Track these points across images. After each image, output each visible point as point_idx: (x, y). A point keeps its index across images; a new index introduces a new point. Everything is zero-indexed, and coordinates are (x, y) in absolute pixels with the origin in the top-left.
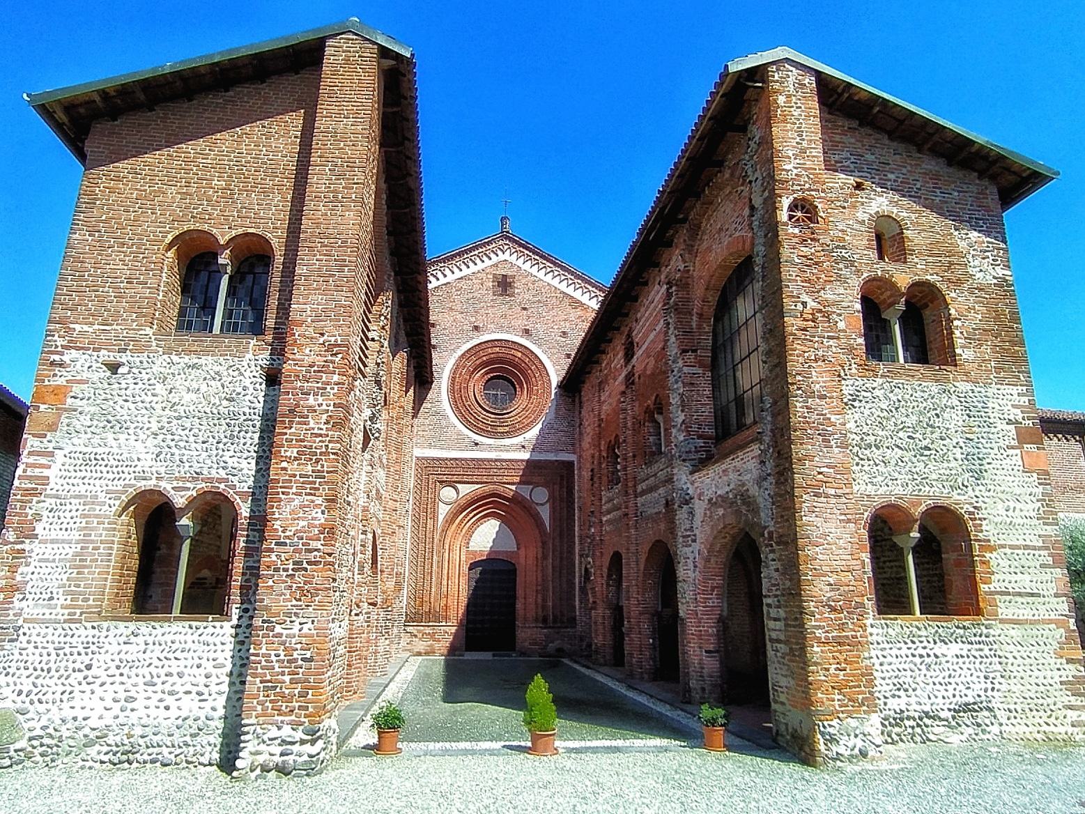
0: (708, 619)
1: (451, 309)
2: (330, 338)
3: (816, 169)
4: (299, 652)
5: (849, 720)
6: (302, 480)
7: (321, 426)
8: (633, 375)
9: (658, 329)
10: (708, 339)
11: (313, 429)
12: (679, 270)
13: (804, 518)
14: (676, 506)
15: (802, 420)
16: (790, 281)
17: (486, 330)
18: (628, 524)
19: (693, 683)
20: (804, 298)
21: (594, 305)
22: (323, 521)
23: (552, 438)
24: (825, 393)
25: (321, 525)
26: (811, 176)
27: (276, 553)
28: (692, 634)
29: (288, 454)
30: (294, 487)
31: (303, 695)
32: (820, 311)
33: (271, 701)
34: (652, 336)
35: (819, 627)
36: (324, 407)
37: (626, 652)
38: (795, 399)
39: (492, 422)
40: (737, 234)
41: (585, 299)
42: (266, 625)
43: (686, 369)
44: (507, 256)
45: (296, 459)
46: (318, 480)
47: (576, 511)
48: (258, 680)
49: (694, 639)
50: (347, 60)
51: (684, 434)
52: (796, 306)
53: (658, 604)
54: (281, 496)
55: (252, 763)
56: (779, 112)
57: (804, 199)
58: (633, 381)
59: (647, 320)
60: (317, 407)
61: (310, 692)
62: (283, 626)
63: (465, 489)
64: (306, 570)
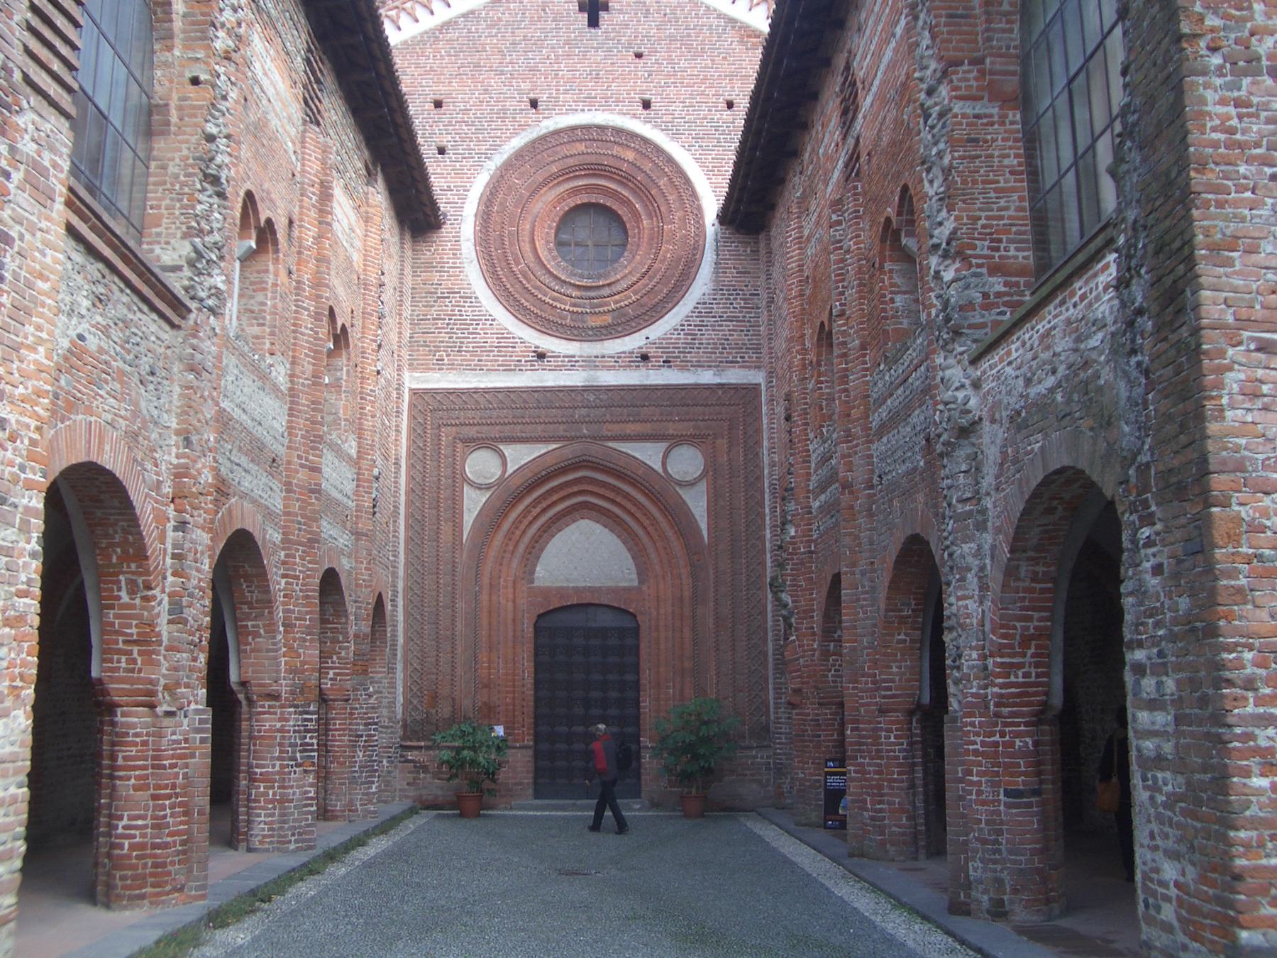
0: (1012, 715)
1: (477, 66)
10: (1011, 31)
13: (1229, 414)
15: (1222, 137)
17: (555, 105)
19: (975, 870)
23: (708, 336)
28: (976, 752)
34: (888, 54)
38: (1201, 80)
39: (574, 305)
43: (958, 108)
47: (767, 496)
51: (957, 265)
53: (920, 688)
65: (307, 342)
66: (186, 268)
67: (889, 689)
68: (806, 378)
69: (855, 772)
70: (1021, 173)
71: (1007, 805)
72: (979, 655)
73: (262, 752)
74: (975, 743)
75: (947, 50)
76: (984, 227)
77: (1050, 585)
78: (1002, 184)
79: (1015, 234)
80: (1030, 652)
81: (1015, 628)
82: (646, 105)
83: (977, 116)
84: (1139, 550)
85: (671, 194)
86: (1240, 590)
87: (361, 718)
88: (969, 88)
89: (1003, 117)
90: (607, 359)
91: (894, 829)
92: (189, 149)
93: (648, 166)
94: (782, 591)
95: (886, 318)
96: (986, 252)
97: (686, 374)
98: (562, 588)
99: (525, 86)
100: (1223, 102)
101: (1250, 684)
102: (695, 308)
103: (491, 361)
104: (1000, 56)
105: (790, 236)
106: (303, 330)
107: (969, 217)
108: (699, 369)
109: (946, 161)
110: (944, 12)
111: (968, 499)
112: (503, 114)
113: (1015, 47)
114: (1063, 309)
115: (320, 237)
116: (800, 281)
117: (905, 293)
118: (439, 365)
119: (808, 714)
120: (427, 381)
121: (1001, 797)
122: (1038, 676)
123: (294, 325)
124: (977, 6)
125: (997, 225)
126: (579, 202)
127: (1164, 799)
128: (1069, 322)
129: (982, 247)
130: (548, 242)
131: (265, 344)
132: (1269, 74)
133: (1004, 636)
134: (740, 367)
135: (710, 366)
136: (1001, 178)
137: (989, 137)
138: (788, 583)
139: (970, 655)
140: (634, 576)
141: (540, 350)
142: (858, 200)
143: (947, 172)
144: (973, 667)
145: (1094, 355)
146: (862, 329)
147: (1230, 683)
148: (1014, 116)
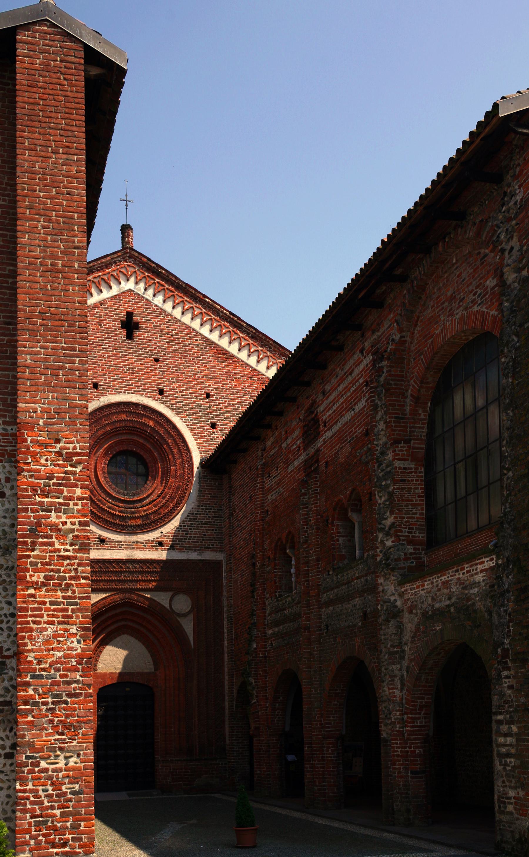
0: (415, 739)
2: (67, 445)
7: (68, 547)
8: (317, 461)
9: (358, 408)
10: (423, 428)
11: (59, 550)
12: (393, 340)
14: (380, 620)
18: (309, 639)
22: (79, 651)
25: (78, 655)
27: (32, 687)
28: (398, 756)
29: (34, 579)
30: (45, 616)
31: (75, 828)
33: (44, 835)
34: (347, 417)
36: (69, 526)
37: (306, 780)
39: (121, 512)
40: (475, 308)
42: (30, 761)
43: (397, 464)
44: (130, 285)
45: (44, 584)
46: (70, 607)
47: (225, 623)
48: (28, 815)
49: (399, 760)
50: (46, 64)
51: (393, 539)
54: (32, 625)
58: (317, 468)
59: (340, 395)
60: (61, 526)
61: (82, 823)
62: (49, 761)
64: (66, 702)
67: (329, 727)
68: (264, 565)
69: (309, 768)
71: (412, 778)
72: (400, 714)
74: (397, 751)
75: (393, 434)
76: (406, 522)
77: (432, 684)
78: (414, 502)
80: (423, 712)
81: (417, 702)
82: (161, 392)
83: (405, 469)
84: (502, 680)
85: (175, 449)
89: (416, 469)
90: (139, 544)
91: (331, 794)
93: (161, 431)
94: (249, 677)
95: (334, 549)
96: (406, 534)
97: (183, 554)
98: (112, 673)
102: (188, 516)
104: (418, 440)
107: (400, 517)
108: (190, 551)
109: (391, 489)
110: (393, 416)
111: (396, 646)
113: (424, 436)
114: (457, 574)
116: (262, 512)
117: (343, 536)
119: (263, 740)
121: (409, 774)
122: (425, 722)
124: (408, 414)
125: (412, 521)
126: (121, 449)
127: (510, 768)
128: (459, 579)
130: (104, 473)
133: (413, 706)
134: (211, 551)
135: (195, 550)
136: (414, 499)
137: (410, 479)
138: (253, 672)
139: (396, 714)
140: (152, 666)
141: (102, 537)
142: (317, 484)
143: (391, 494)
144: (397, 719)
145: (473, 597)
146: (318, 551)
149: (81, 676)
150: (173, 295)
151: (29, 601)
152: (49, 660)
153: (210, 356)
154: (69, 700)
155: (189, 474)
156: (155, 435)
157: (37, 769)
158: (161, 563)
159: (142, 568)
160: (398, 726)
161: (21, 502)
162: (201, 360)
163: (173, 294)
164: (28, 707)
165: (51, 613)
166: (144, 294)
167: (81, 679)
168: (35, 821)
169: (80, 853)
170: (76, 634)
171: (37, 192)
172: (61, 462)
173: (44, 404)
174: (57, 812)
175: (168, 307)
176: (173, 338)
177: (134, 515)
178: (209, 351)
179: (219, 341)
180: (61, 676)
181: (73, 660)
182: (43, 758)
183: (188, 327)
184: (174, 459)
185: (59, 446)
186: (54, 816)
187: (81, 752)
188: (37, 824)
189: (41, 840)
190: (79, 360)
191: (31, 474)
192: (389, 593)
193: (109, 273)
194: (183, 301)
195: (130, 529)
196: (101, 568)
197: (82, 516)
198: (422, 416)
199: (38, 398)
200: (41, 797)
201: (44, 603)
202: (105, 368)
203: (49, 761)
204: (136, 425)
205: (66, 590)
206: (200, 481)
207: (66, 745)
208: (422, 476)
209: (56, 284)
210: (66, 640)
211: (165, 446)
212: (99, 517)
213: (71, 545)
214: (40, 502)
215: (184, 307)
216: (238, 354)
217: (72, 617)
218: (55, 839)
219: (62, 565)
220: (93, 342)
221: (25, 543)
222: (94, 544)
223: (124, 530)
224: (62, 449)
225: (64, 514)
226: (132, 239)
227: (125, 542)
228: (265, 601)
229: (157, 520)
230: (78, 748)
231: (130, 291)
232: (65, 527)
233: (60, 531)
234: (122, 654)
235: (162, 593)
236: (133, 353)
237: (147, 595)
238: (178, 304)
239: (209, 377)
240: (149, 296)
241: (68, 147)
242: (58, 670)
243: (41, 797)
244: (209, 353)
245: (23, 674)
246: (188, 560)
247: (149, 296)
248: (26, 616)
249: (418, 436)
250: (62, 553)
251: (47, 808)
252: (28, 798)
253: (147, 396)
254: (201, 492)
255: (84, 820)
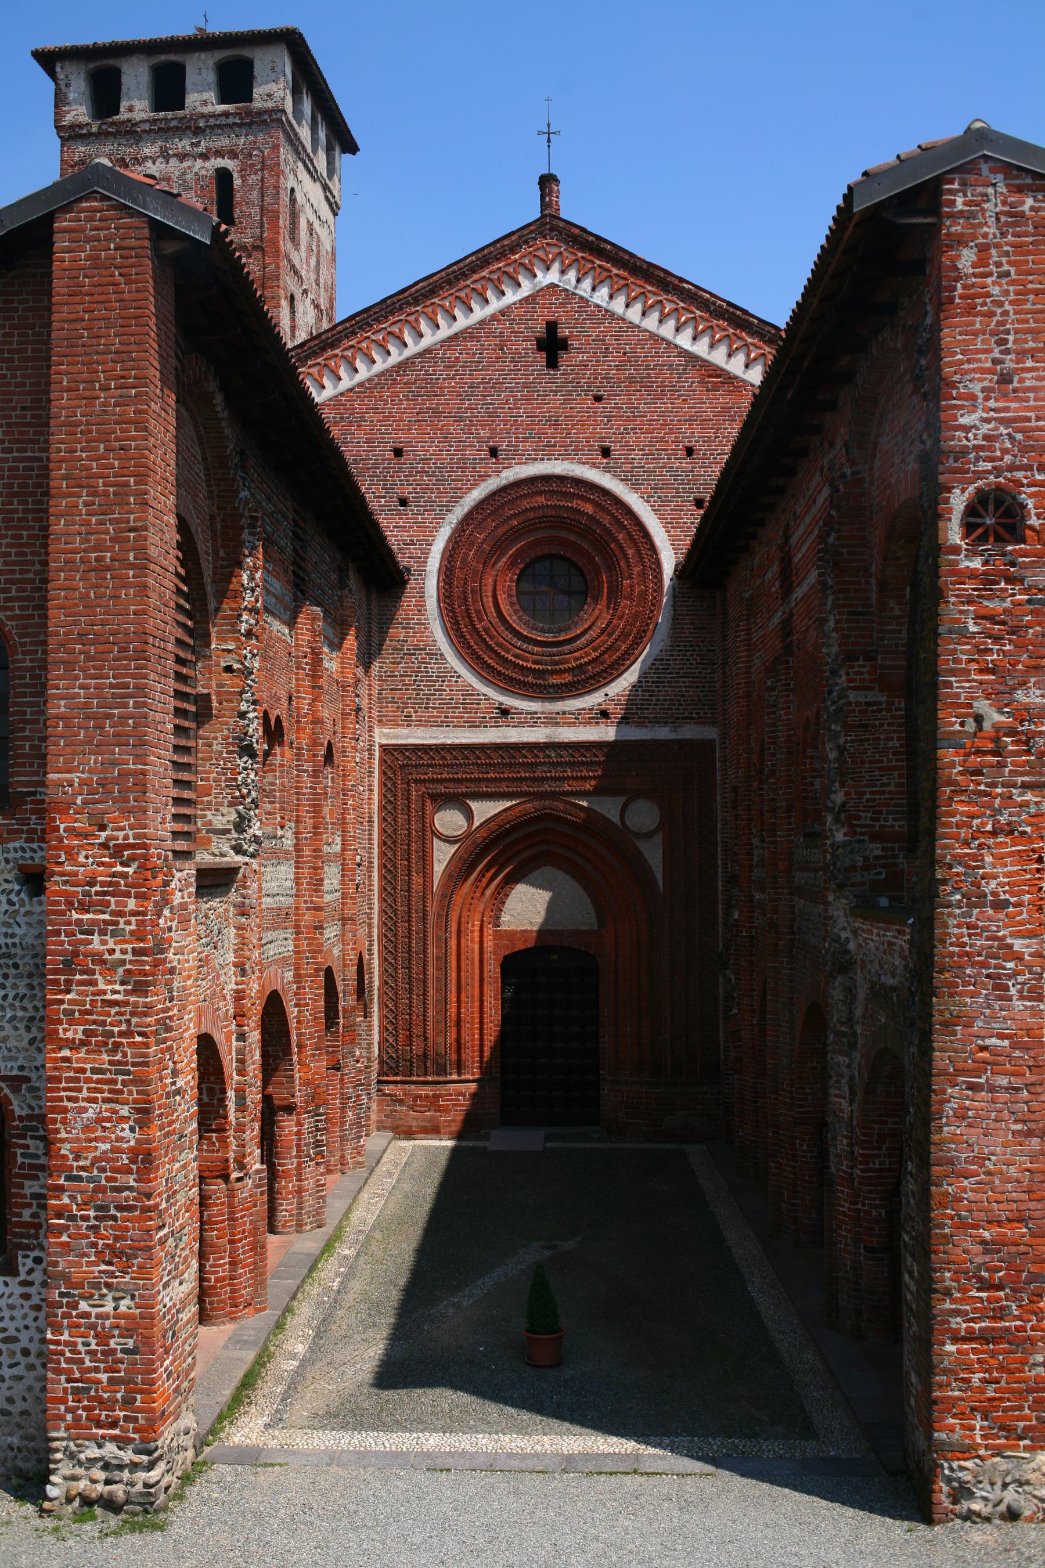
3: (1028, 419)
4: (117, 1340)
5: (997, 1459)
6: (95, 1077)
7: (117, 987)
10: (900, 632)
11: (104, 992)
13: (946, 1129)
15: (956, 949)
16: (954, 672)
20: (982, 706)
21: (755, 376)
22: (132, 1143)
24: (1007, 896)
25: (131, 1150)
26: (1019, 436)
29: (70, 1035)
30: (85, 1090)
32: (1012, 732)
33: (85, 1408)
35: (957, 1313)
36: (118, 955)
38: (946, 911)
39: (535, 662)
41: (736, 366)
42: (65, 1300)
43: (852, 696)
44: (553, 276)
45: (83, 1043)
46: (120, 1078)
48: (63, 1378)
51: (845, 830)
52: (962, 724)
54: (66, 1103)
55: (68, 1491)
56: (960, 290)
57: (999, 487)
60: (107, 956)
61: (139, 1397)
62: (91, 1302)
63: (484, 810)
64: (114, 1218)
65: (308, 800)
66: (233, 831)
67: (803, 1106)
70: (902, 753)
73: (282, 1153)
74: (844, 1207)
76: (868, 800)
78: (885, 764)
79: (894, 806)
80: (885, 1146)
81: (874, 1129)
82: (606, 452)
83: (868, 704)
86: (945, 1236)
87: (350, 1082)
88: (863, 680)
89: (890, 704)
91: (805, 1221)
92: (229, 730)
93: (606, 521)
96: (868, 822)
97: (644, 731)
98: (526, 931)
99: (484, 433)
100: (959, 926)
101: (947, 1292)
102: (653, 664)
103: (457, 717)
105: (739, 636)
106: (304, 790)
107: (856, 793)
110: (845, 610)
112: (463, 463)
113: (903, 645)
115: (314, 700)
118: (408, 721)
120: (396, 737)
121: (862, 1250)
122: (890, 1164)
123: (297, 788)
126: (540, 553)
129: (866, 818)
130: (510, 596)
131: (276, 819)
132: (991, 907)
134: (695, 723)
137: (877, 722)
140: (594, 920)
147: (936, 1291)
148: (899, 703)
149: (135, 1180)
150: (627, 285)
151: (62, 1067)
152: (91, 1155)
153: (692, 382)
154: (119, 1215)
155: (655, 591)
156: (594, 527)
157: (74, 1313)
158: (605, 746)
159: (573, 757)
160: (845, 1163)
161: (50, 920)
162: (677, 391)
163: (625, 282)
164: (62, 1221)
165: (93, 1085)
166: (576, 288)
167: (135, 1184)
168: (72, 1387)
169: (134, 1439)
170: (129, 1118)
171: (79, 453)
172: (107, 859)
173: (83, 772)
174: (104, 1377)
175: (618, 306)
176: (628, 358)
177: (557, 667)
178: (691, 373)
179: (709, 354)
180: (108, 1179)
181: (124, 1156)
182: (83, 1297)
183: (654, 337)
184: (629, 566)
185: (103, 834)
186: (99, 1382)
187: (137, 1293)
188: (76, 1391)
189: (81, 1416)
190: (134, 702)
191: (64, 878)
192: (840, 926)
193: (516, 261)
194: (643, 293)
195: (551, 690)
196: (503, 758)
197: (137, 939)
198: (897, 612)
199: (76, 763)
200: (80, 1353)
201: (83, 1071)
202: (509, 421)
203: (91, 1302)
204: (561, 513)
205: (114, 1051)
206: (674, 601)
207: (115, 1280)
208: (901, 717)
209: (103, 590)
210: (115, 1126)
211: (612, 546)
212: (499, 673)
213: (122, 983)
214: (77, 919)
215: (646, 302)
216: (744, 373)
217: (121, 1092)
218: (100, 1415)
219: (108, 1014)
220: (490, 379)
221: (56, 982)
222: (490, 718)
223: (541, 692)
224: (109, 839)
225: (112, 937)
226: (557, 197)
227: (542, 713)
228: (750, 839)
229: (598, 674)
230: (131, 1287)
231: (552, 286)
232: (113, 957)
233: (106, 964)
234: (543, 897)
235: (606, 799)
236: (556, 391)
237: (581, 803)
238: (635, 298)
239: (691, 420)
240: (585, 291)
241: (123, 378)
242: (103, 1170)
243: (80, 1353)
244: (691, 379)
245: (55, 1174)
246: (653, 740)
247: (585, 291)
248: (58, 1090)
249: (891, 646)
250: (108, 997)
251: (89, 1370)
252: (62, 1353)
253: (581, 462)
254: (676, 620)
255: (141, 1392)
